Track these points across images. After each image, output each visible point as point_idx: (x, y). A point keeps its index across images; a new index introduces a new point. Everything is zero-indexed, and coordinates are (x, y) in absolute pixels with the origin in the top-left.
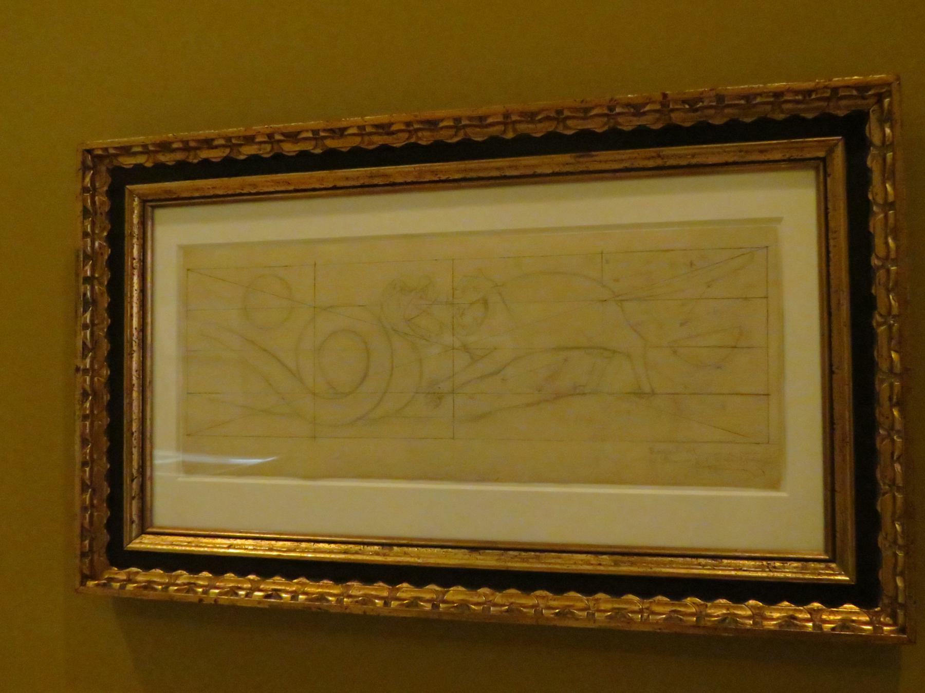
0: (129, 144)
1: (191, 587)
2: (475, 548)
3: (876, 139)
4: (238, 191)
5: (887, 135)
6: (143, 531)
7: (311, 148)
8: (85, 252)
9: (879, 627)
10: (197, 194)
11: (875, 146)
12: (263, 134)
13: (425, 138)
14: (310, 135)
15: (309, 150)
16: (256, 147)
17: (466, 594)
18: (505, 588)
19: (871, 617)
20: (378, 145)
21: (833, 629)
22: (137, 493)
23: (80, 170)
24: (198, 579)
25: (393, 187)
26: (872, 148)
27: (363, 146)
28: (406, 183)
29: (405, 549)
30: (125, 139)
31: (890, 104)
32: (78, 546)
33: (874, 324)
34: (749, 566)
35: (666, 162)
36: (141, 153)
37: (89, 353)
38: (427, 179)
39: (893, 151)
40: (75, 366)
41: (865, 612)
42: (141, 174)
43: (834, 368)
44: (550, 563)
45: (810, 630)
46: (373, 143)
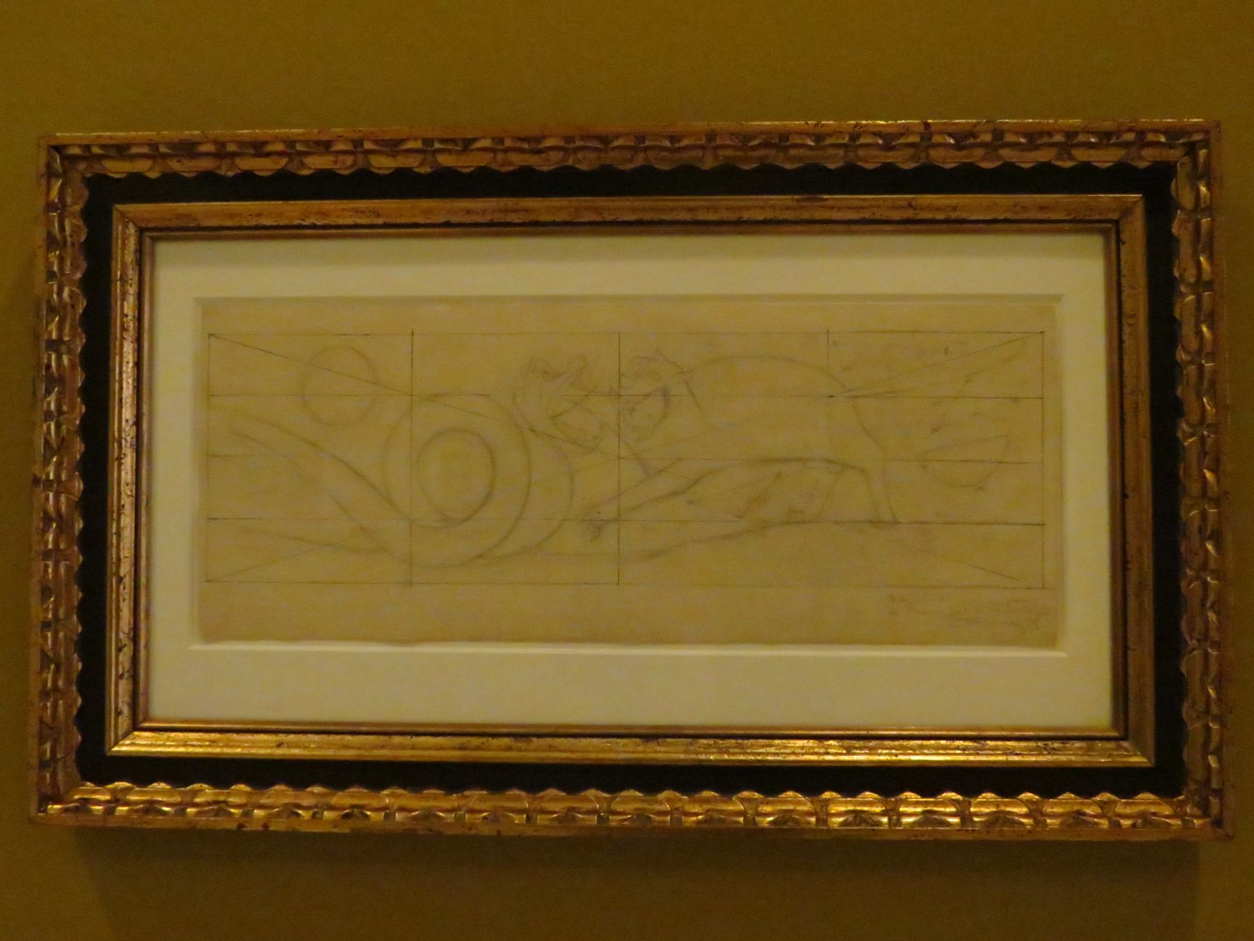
0: (125, 142)
1: (220, 808)
2: (651, 735)
3: (1187, 200)
4: (296, 222)
5: (1202, 196)
6: (135, 726)
7: (415, 165)
8: (48, 302)
9: (1189, 820)
10: (228, 223)
11: (1183, 209)
12: (346, 139)
13: (586, 162)
14: (145, 150)
15: (412, 168)
16: (331, 158)
17: (644, 801)
18: (347, 787)
19: (1175, 807)
20: (516, 167)
21: (844, 824)
22: (126, 669)
23: (42, 176)
24: (229, 795)
25: (535, 227)
26: (1179, 212)
27: (495, 167)
28: (554, 223)
29: (549, 741)
30: (122, 134)
31: (1208, 156)
32: (35, 753)
33: (1180, 435)
34: (1020, 748)
35: (917, 214)
36: (281, 154)
37: (53, 456)
38: (586, 219)
39: (1210, 216)
40: (32, 478)
41: (1166, 802)
42: (138, 189)
43: (1128, 492)
44: (759, 754)
45: (1105, 827)
46: (511, 164)
